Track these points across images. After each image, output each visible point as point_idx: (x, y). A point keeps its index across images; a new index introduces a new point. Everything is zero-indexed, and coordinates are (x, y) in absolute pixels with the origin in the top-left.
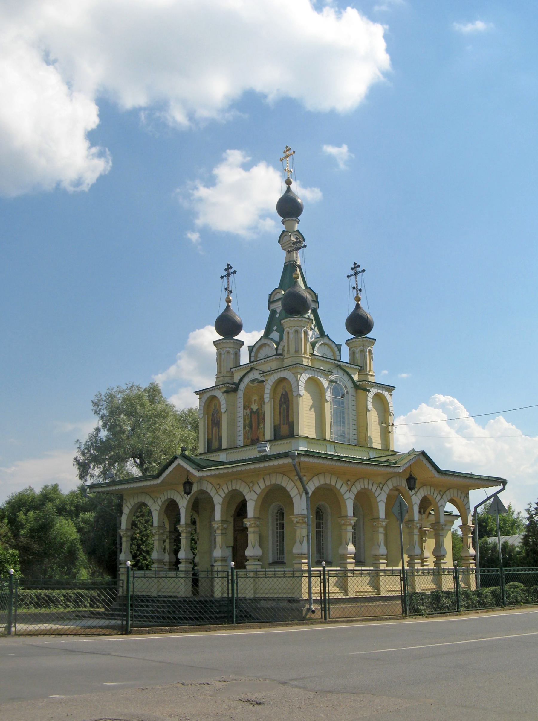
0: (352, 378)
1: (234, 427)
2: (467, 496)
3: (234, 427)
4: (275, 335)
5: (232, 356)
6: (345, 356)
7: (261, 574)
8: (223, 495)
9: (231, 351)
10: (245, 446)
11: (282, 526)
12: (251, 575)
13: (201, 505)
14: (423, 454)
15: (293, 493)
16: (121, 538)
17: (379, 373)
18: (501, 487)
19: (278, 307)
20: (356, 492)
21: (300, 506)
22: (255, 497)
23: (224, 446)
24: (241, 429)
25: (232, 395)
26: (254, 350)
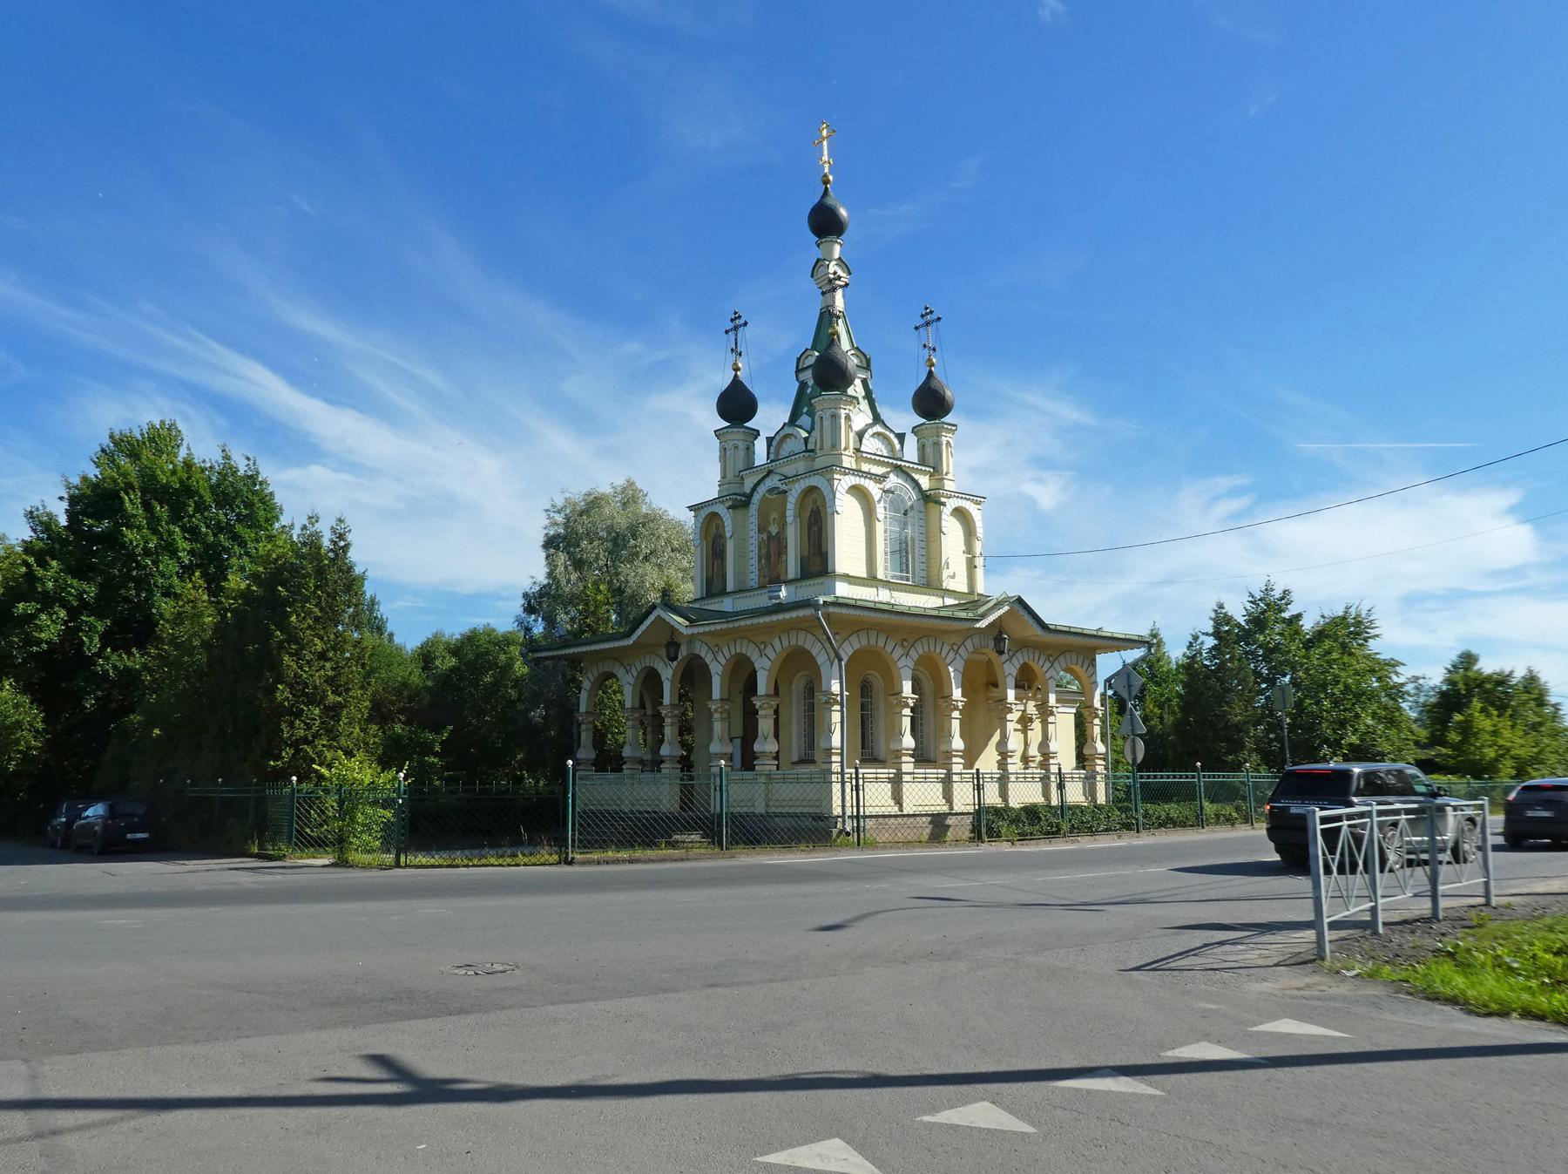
0: (916, 484)
1: (742, 562)
2: (1093, 663)
3: (742, 562)
4: (805, 420)
5: (742, 453)
6: (911, 451)
9: (741, 445)
12: (763, 779)
13: (694, 675)
14: (1020, 601)
15: (821, 659)
16: (579, 725)
19: (808, 376)
20: (916, 657)
22: (768, 664)
23: (730, 587)
24: (754, 561)
25: (741, 512)
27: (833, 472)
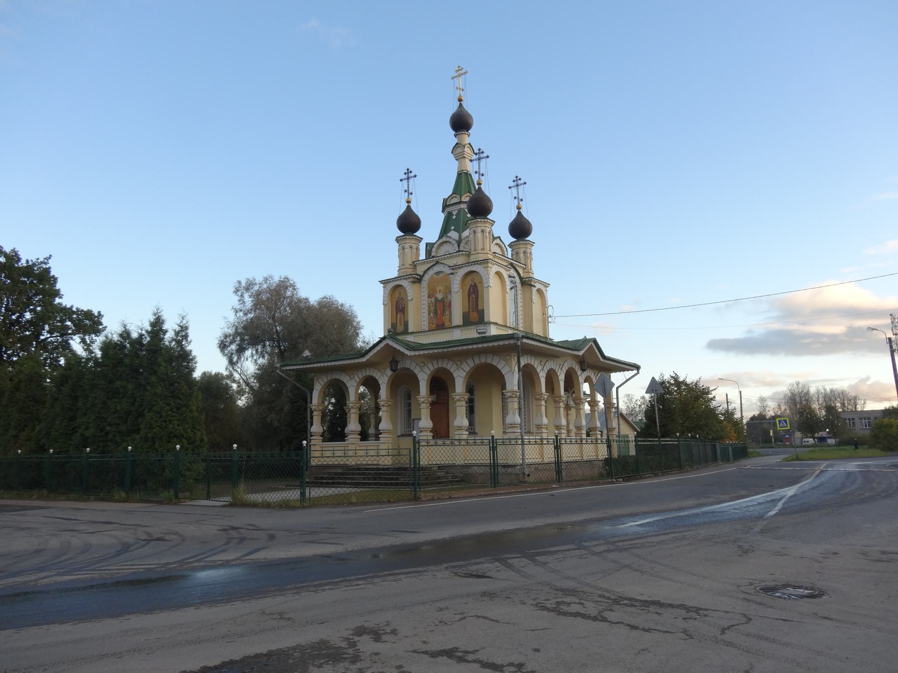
1: (418, 316)
3: (418, 316)
7: (584, 442)
8: (429, 373)
10: (429, 331)
11: (409, 405)
14: (595, 341)
16: (312, 412)
17: (539, 270)
18: (635, 372)
21: (562, 377)
26: (436, 246)
27: (487, 262)
